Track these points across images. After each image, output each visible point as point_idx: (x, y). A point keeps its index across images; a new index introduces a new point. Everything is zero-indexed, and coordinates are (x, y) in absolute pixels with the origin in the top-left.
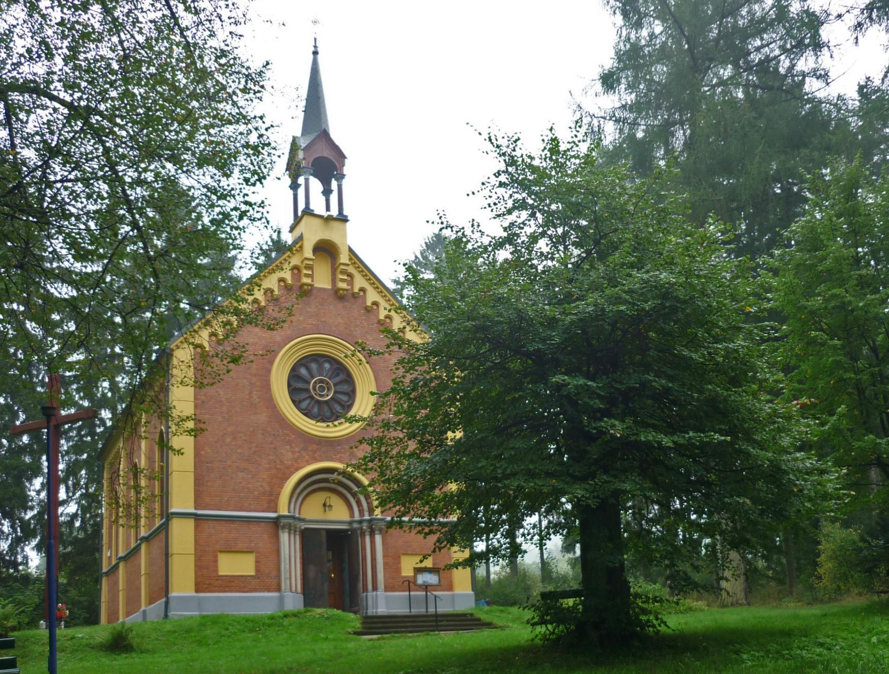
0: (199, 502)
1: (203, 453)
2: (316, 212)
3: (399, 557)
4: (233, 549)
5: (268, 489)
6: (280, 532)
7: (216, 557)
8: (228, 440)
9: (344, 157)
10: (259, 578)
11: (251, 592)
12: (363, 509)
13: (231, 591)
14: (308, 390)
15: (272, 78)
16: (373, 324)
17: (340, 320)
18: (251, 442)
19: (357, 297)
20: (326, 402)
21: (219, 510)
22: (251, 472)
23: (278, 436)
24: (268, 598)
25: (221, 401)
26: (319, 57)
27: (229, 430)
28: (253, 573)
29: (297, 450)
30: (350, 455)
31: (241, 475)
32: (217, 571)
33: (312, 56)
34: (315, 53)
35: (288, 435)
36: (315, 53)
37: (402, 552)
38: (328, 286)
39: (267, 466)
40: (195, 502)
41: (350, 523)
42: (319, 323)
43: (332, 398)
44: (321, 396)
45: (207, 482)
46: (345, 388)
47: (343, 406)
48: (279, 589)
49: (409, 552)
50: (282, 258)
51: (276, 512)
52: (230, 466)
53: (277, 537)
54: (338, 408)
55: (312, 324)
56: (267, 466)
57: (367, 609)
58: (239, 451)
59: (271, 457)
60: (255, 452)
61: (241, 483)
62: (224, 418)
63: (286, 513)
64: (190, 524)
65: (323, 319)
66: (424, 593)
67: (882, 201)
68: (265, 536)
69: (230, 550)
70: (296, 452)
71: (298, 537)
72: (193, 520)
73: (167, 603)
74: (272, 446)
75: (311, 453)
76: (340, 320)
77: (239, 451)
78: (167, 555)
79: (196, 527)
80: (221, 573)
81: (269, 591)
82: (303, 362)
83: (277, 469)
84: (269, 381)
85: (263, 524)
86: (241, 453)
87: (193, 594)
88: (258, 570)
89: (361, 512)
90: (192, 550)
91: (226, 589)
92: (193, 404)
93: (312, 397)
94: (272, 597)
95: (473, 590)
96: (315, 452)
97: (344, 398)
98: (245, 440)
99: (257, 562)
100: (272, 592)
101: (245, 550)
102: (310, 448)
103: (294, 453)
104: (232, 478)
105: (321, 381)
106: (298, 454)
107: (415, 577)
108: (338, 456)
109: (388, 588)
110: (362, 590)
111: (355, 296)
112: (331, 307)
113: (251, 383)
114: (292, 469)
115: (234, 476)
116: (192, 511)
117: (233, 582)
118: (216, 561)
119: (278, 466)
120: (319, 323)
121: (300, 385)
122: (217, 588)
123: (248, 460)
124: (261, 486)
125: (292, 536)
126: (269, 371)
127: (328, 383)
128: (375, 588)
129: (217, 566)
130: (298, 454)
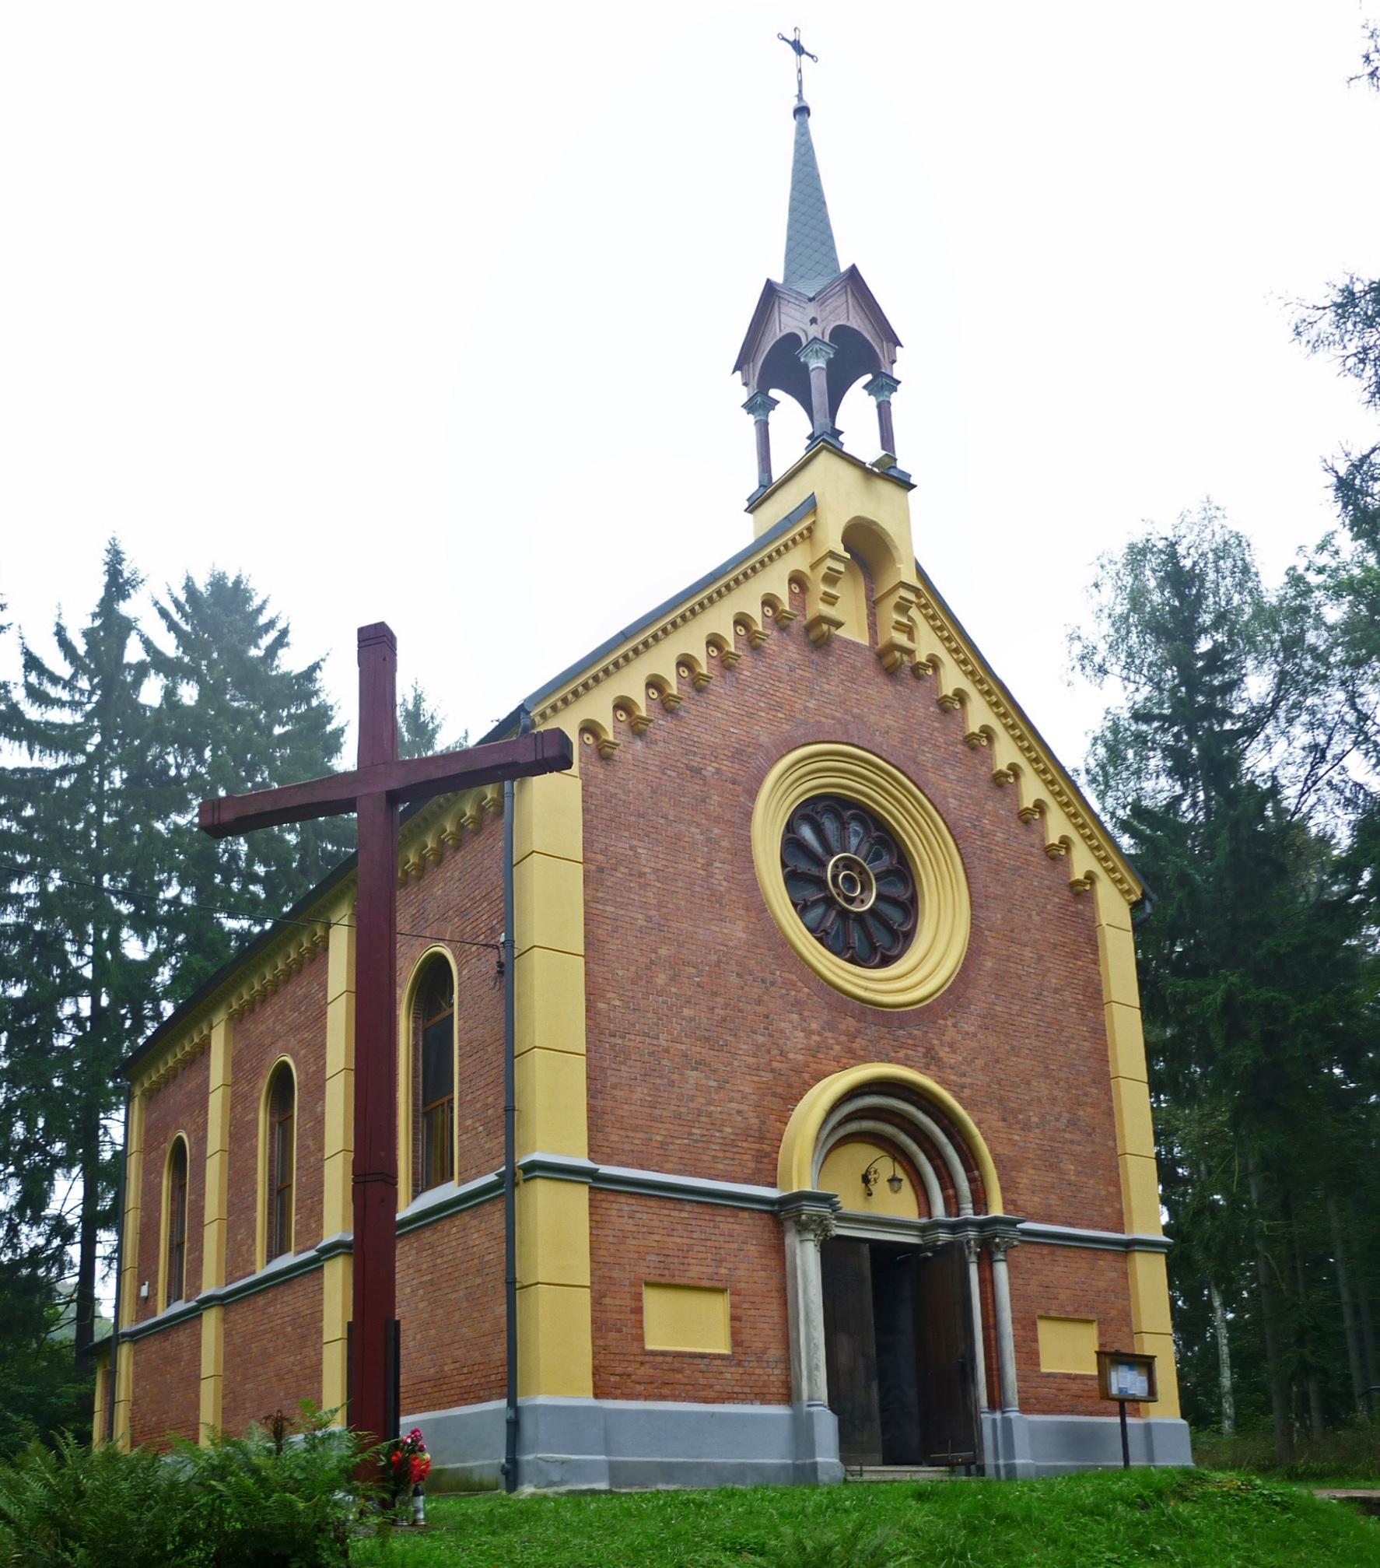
1: (601, 1005)
2: (845, 449)
3: (1034, 1324)
4: (677, 1280)
5: (754, 1121)
6: (791, 1239)
7: (638, 1297)
8: (661, 979)
9: (898, 343)
10: (739, 1364)
11: (723, 1401)
12: (956, 1196)
13: (675, 1398)
14: (821, 883)
16: (954, 744)
17: (889, 720)
18: (715, 994)
19: (923, 672)
20: (860, 916)
22: (715, 1071)
23: (773, 984)
24: (764, 1418)
25: (642, 875)
26: (812, 122)
27: (663, 952)
28: (725, 1349)
29: (814, 1026)
30: (925, 1055)
32: (640, 1338)
33: (792, 124)
34: (802, 111)
35: (793, 984)
36: (802, 111)
37: (1041, 1312)
38: (864, 640)
41: (923, 1230)
42: (849, 718)
43: (871, 910)
45: (614, 1087)
46: (899, 892)
47: (894, 934)
48: (789, 1395)
49: (1053, 1314)
50: (790, 535)
51: (773, 1185)
52: (667, 1051)
53: (779, 1252)
54: (882, 938)
55: (833, 718)
57: (1010, 1452)
58: (686, 1012)
59: (761, 1039)
60: (724, 1020)
61: (692, 1098)
62: (649, 919)
63: (808, 1188)
64: (578, 1196)
65: (856, 711)
66: (1117, 1420)
68: (752, 1249)
70: (812, 1032)
72: (586, 1188)
73: (514, 1427)
75: (843, 1038)
76: (889, 720)
77: (686, 1012)
79: (593, 1207)
81: (765, 1401)
82: (808, 810)
83: (773, 1071)
84: (749, 839)
85: (745, 1215)
86: (692, 1019)
87: (589, 1401)
88: (736, 1342)
89: (952, 1203)
91: (665, 1391)
92: (579, 869)
93: (829, 902)
94: (774, 1417)
95: (1183, 1416)
96: (852, 1037)
97: (895, 915)
98: (698, 985)
100: (769, 1402)
101: (705, 1283)
102: (842, 1027)
104: (672, 1083)
106: (816, 1038)
107: (1103, 1377)
108: (901, 1054)
109: (1026, 1407)
110: (984, 1401)
112: (872, 691)
113: (709, 840)
114: (806, 1076)
115: (675, 1077)
116: (585, 1162)
117: (680, 1371)
118: (639, 1311)
119: (775, 1064)
120: (849, 718)
121: (804, 866)
122: (640, 1388)
123: (707, 1039)
124: (739, 1112)
126: (748, 815)
127: (863, 872)
128: (997, 1401)
129: (640, 1324)
130: (816, 1038)
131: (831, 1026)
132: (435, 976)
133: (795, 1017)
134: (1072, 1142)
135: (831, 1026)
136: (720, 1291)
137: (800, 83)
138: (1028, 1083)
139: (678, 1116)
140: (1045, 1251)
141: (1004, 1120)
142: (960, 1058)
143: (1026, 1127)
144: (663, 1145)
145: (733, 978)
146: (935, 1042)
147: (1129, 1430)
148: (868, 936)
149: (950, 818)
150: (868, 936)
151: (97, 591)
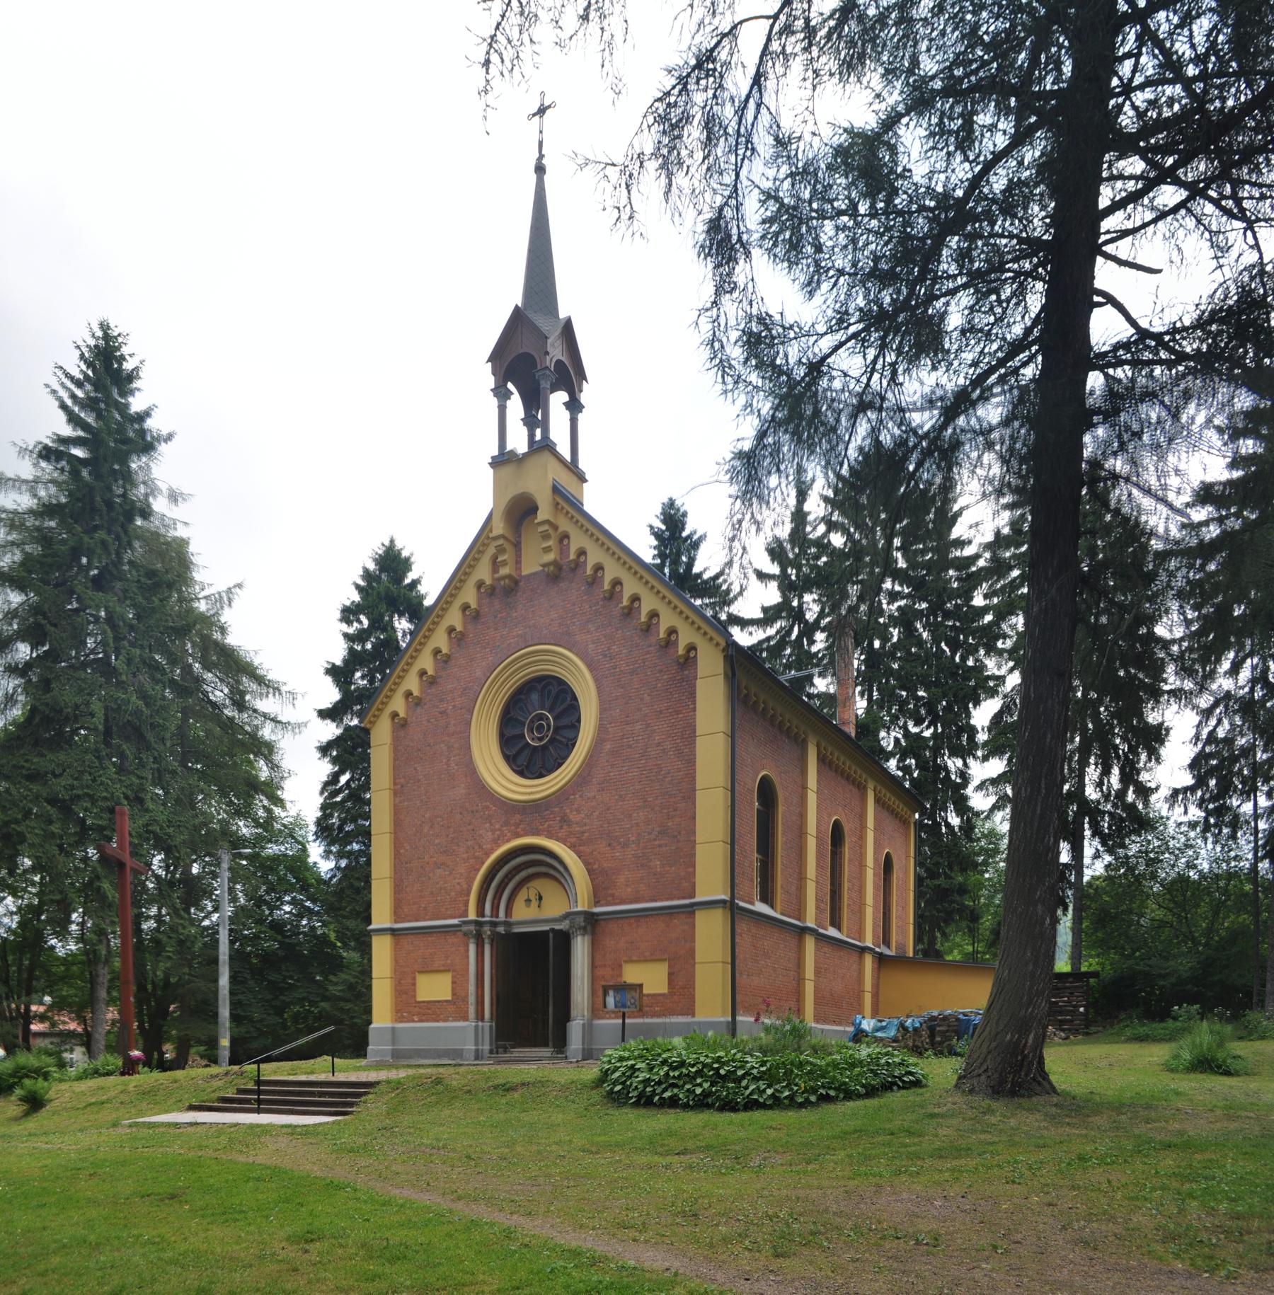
0: (398, 914)
3: (621, 966)
7: (414, 979)
15: (173, 507)
21: (417, 920)
31: (438, 872)
32: (415, 996)
34: (540, 169)
35: (487, 807)
36: (540, 169)
39: (465, 856)
40: (395, 913)
44: (549, 726)
56: (465, 856)
59: (469, 843)
67: (847, 177)
69: (428, 970)
74: (470, 827)
78: (732, 844)
80: (419, 999)
88: (454, 994)
90: (374, 982)
96: (517, 825)
99: (453, 983)
103: (493, 831)
118: (414, 984)
129: (414, 990)
131: (507, 823)
132: (240, 1091)
133: (487, 825)
134: (660, 846)
135: (507, 823)
136: (448, 971)
137: (541, 144)
138: (630, 816)
139: (432, 893)
140: (632, 921)
143: (625, 845)
144: (425, 909)
145: (458, 816)
147: (739, 1026)
148: (565, 727)
149: (208, 1097)
150: (565, 727)
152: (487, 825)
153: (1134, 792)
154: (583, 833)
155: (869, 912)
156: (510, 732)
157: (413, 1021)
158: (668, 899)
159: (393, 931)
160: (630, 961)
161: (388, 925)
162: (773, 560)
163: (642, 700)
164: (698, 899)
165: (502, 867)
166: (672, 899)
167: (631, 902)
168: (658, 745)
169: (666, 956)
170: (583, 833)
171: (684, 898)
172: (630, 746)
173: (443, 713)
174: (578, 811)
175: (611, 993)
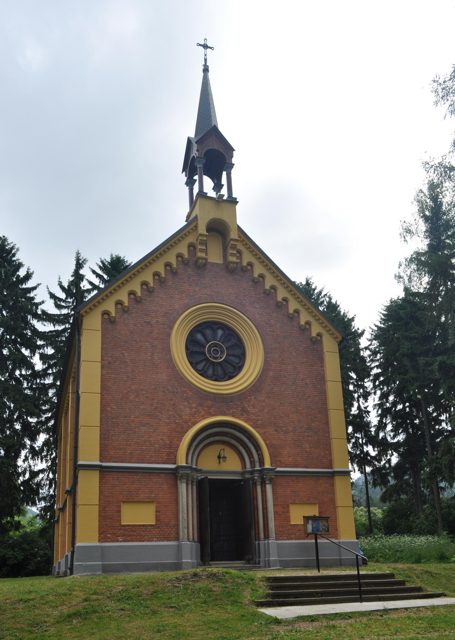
3: (288, 506)
21: (122, 462)
31: (143, 429)
59: (171, 413)
71: (195, 487)
88: (157, 520)
103: (191, 408)
105: (215, 345)
111: (244, 270)
118: (119, 511)
125: (190, 486)
129: (120, 516)
134: (308, 436)
140: (294, 478)
141: (276, 430)
142: (257, 410)
146: (246, 405)
151: (73, 267)
152: (186, 403)
153: (11, 407)
154: (258, 420)
155: (151, 471)
156: (237, 352)
157: (118, 541)
158: (315, 468)
159: (101, 469)
160: (294, 503)
161: (98, 463)
162: (100, 270)
163: (291, 353)
164: (336, 470)
165: (247, 437)
166: (318, 468)
167: (292, 467)
168: (303, 380)
169: (317, 502)
170: (258, 420)
171: (325, 468)
172: (285, 377)
173: (149, 323)
174: (254, 406)
175: (310, 522)
